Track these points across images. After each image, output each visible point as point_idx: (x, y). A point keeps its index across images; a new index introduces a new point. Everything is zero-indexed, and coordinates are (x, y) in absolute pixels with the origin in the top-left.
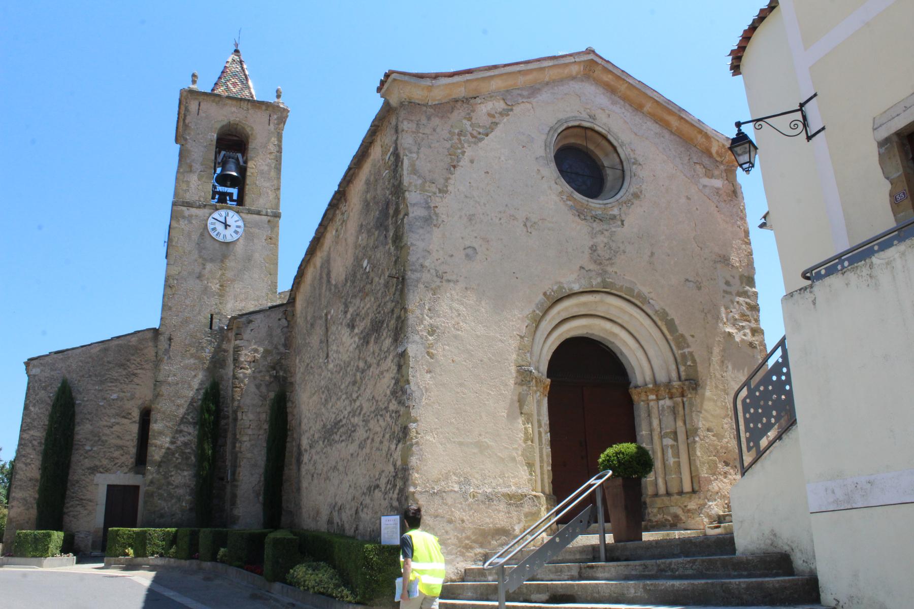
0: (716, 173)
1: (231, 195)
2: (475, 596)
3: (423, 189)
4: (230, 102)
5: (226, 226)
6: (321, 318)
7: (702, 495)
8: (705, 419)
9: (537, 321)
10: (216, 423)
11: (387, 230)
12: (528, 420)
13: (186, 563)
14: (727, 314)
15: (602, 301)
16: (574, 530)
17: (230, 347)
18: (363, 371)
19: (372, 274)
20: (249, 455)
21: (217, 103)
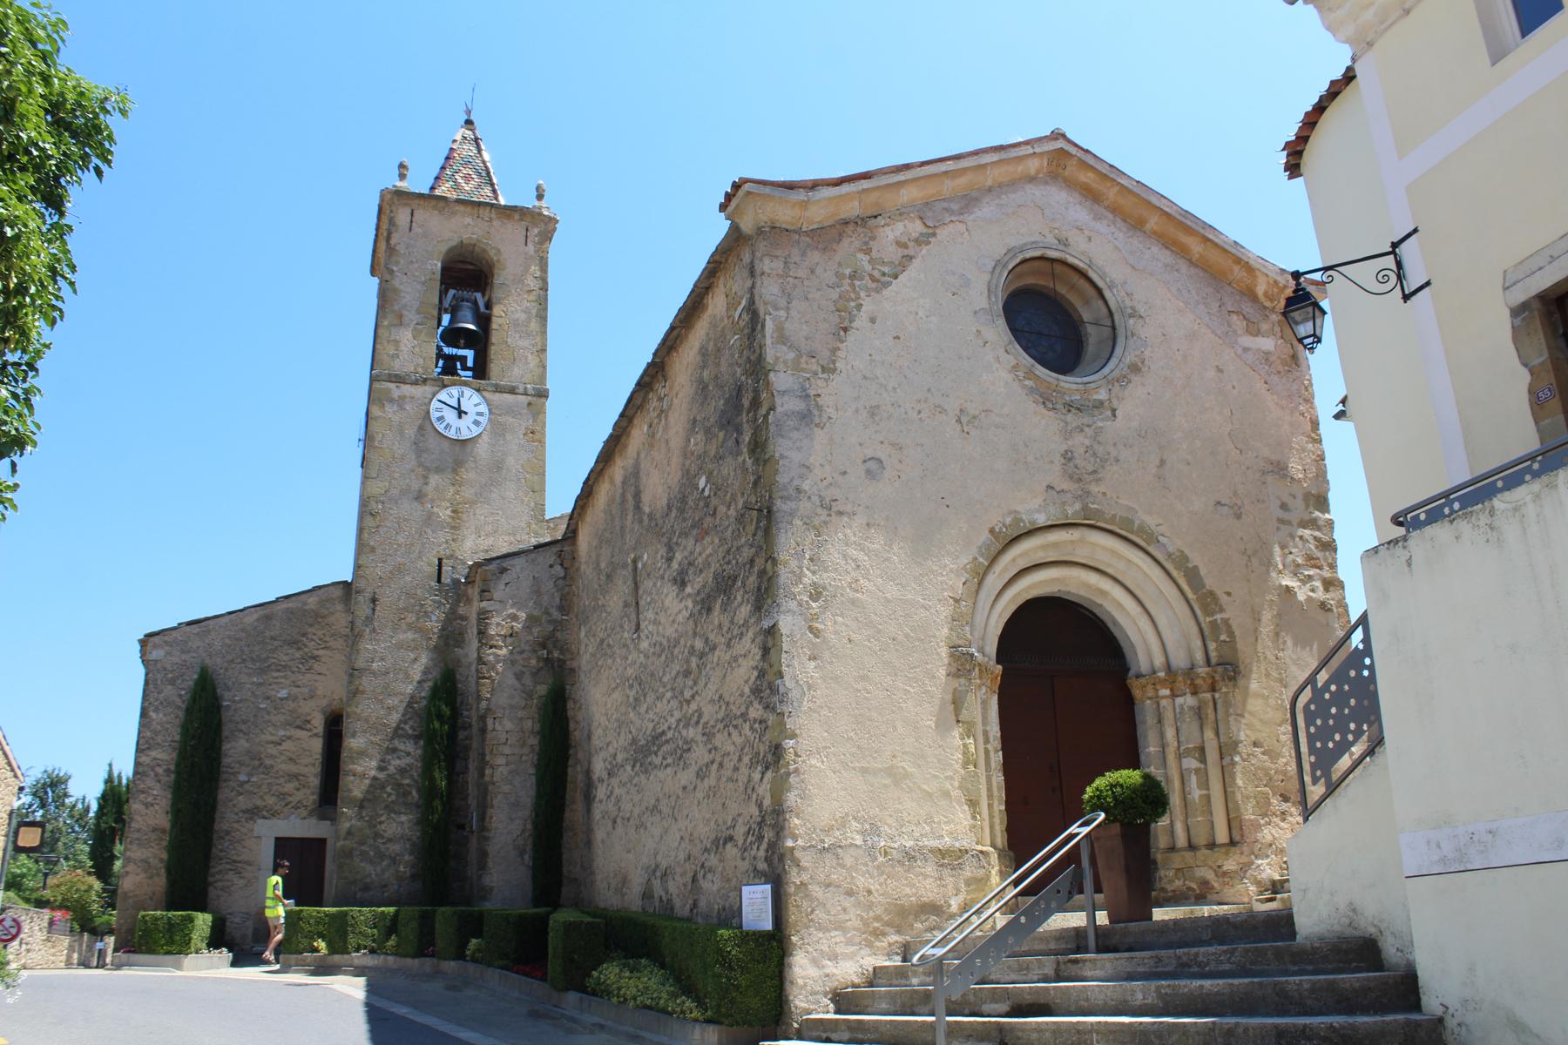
0: (1265, 327)
1: (463, 359)
2: (892, 1009)
3: (797, 367)
4: (461, 208)
5: (461, 413)
6: (625, 566)
7: (1246, 849)
8: (1250, 726)
9: (981, 575)
10: (452, 736)
11: (739, 431)
12: (969, 733)
13: (412, 963)
14: (1284, 556)
15: (1082, 540)
16: (1048, 905)
17: (471, 611)
18: (702, 655)
19: (714, 501)
20: (506, 788)
21: (441, 211)
